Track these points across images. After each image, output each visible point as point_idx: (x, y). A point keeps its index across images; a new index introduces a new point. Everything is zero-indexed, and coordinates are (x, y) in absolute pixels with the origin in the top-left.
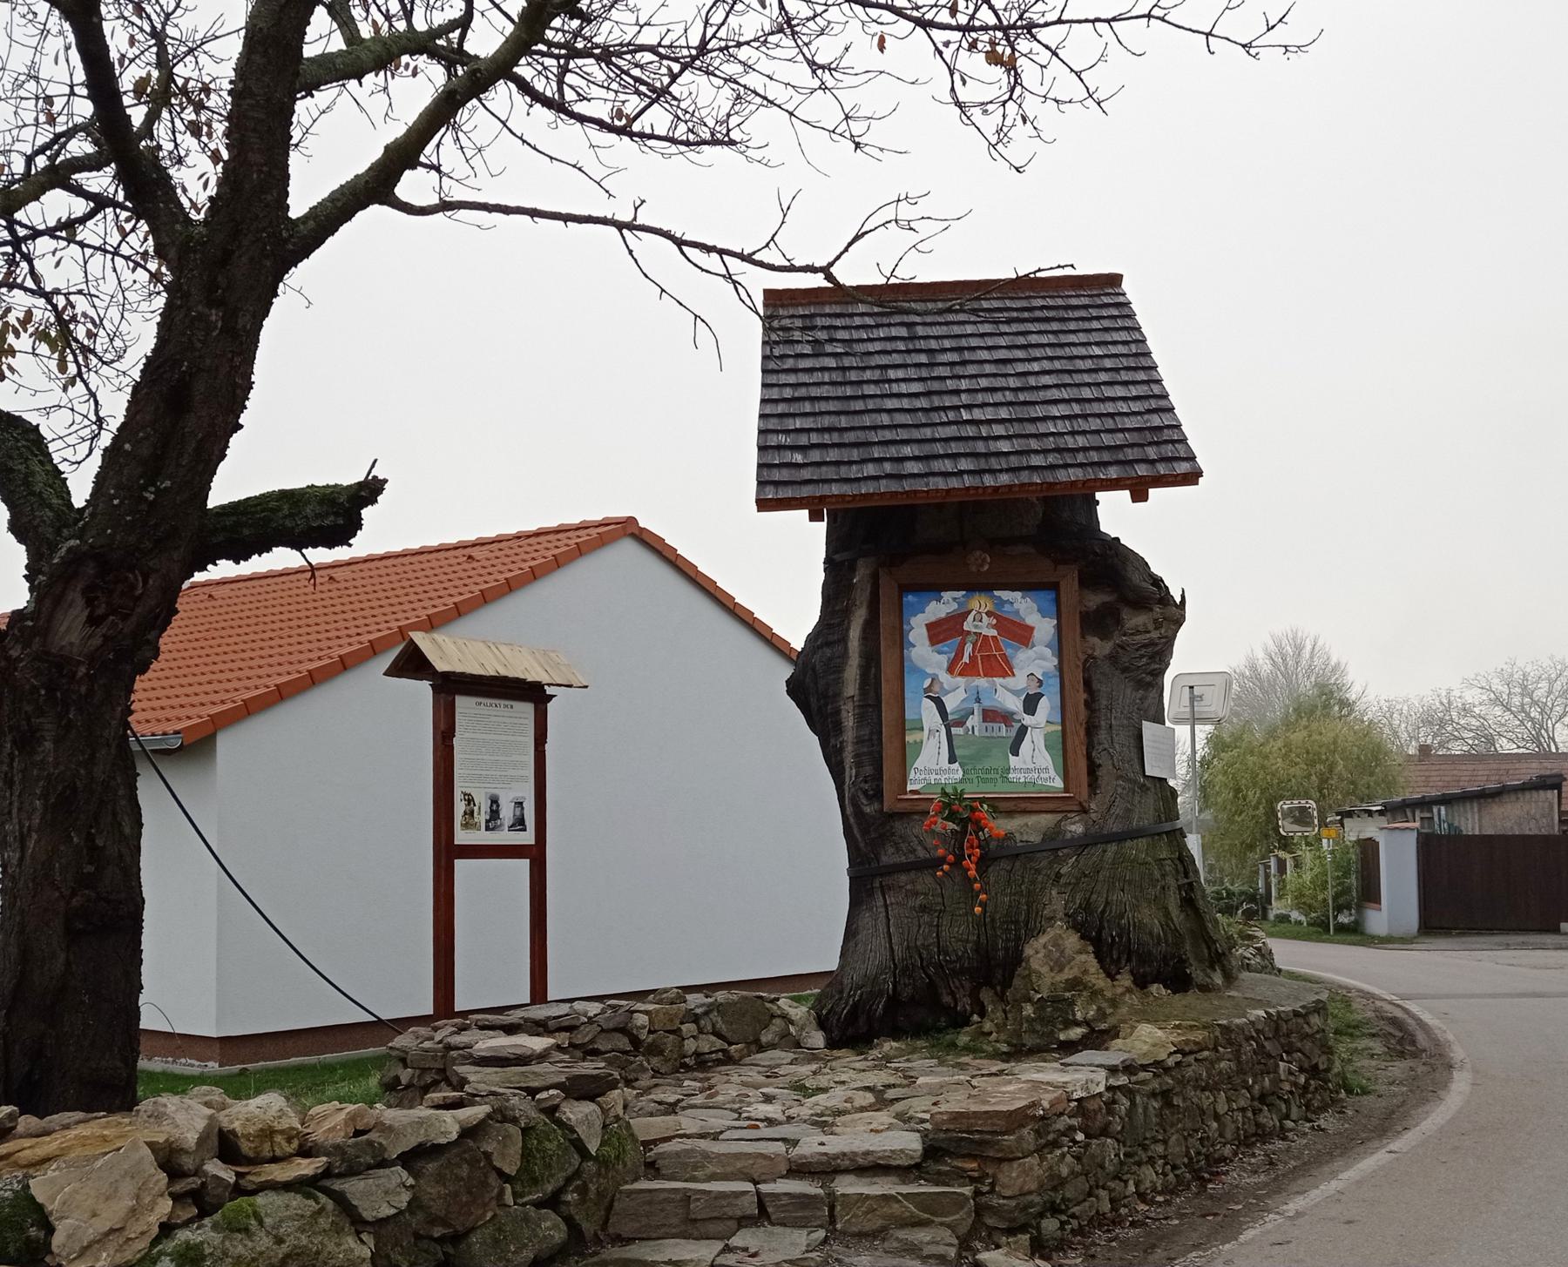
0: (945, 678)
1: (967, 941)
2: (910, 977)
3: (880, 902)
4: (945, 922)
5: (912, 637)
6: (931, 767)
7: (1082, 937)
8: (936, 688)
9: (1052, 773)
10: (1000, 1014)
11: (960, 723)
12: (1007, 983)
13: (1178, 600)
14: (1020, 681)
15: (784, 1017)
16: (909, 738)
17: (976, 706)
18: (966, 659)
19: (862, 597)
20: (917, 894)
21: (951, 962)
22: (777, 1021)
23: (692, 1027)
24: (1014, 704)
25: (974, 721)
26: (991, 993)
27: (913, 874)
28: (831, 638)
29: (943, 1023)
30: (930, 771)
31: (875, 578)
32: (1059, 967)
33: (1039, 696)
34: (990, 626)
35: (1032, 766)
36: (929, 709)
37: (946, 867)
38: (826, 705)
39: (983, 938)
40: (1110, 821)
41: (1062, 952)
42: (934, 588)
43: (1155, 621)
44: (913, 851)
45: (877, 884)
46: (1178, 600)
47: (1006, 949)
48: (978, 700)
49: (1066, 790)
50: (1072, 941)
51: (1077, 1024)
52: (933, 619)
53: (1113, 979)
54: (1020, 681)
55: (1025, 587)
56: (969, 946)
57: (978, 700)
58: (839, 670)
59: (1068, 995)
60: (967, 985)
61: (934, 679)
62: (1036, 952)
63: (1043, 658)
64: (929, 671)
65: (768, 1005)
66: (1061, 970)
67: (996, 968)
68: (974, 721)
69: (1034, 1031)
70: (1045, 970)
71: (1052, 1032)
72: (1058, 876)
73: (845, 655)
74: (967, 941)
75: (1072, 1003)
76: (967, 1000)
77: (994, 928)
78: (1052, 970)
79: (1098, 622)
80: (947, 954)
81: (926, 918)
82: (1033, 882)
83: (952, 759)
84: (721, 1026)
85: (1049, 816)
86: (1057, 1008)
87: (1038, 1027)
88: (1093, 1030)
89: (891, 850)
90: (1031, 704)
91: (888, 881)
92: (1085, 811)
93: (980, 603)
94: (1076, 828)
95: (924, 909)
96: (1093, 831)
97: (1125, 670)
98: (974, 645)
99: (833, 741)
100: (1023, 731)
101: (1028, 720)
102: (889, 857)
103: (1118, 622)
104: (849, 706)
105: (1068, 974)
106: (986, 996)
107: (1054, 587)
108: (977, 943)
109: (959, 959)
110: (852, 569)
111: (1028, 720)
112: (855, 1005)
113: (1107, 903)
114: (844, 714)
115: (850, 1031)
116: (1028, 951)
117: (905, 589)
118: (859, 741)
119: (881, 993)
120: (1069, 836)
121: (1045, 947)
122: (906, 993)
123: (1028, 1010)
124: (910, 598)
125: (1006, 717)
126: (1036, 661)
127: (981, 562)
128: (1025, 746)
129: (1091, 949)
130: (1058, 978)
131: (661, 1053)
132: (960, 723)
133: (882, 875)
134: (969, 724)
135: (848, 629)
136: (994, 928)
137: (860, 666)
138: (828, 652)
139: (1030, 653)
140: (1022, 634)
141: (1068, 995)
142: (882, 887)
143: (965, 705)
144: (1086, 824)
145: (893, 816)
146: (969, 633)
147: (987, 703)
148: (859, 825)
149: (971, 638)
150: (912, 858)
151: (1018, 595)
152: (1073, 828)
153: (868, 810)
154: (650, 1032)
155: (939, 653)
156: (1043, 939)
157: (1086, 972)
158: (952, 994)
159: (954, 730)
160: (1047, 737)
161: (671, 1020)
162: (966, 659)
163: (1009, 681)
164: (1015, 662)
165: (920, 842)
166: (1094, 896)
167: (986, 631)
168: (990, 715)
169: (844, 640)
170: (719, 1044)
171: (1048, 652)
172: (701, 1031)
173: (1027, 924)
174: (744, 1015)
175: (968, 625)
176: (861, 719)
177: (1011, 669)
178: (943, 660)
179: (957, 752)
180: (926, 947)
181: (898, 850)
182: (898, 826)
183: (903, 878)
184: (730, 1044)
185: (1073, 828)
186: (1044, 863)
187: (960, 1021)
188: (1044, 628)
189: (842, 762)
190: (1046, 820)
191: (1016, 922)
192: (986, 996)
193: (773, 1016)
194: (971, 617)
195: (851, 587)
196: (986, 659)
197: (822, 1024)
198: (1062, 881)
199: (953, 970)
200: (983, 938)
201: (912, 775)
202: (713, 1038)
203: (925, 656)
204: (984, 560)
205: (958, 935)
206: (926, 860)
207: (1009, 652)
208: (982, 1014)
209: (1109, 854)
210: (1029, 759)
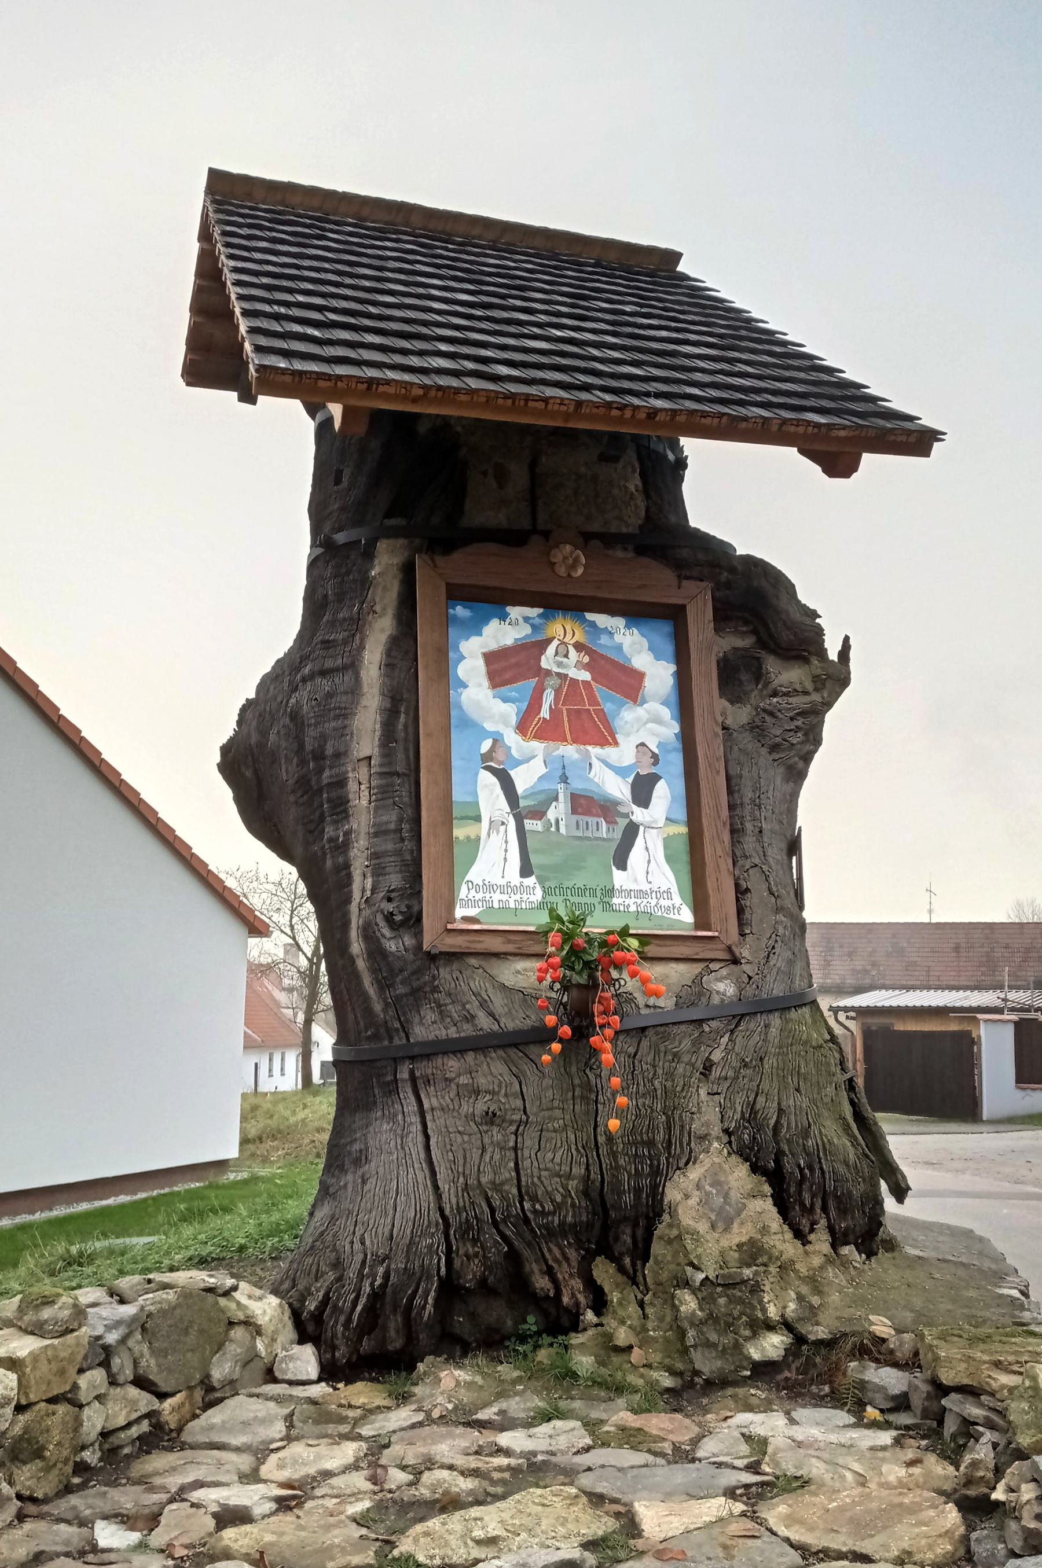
0: (512, 739)
1: (569, 1176)
2: (475, 1241)
3: (411, 1106)
4: (529, 1141)
5: (462, 671)
6: (491, 881)
7: (755, 1169)
8: (500, 755)
9: (677, 900)
10: (633, 1309)
11: (539, 814)
12: (642, 1252)
13: (833, 655)
14: (625, 753)
15: (248, 1323)
16: (459, 832)
17: (561, 788)
18: (545, 713)
19: (385, 597)
20: (477, 1092)
21: (543, 1213)
22: (238, 1333)
23: (98, 1375)
24: (619, 789)
25: (557, 811)
26: (612, 1268)
27: (470, 1057)
28: (329, 664)
29: (532, 1322)
30: (491, 887)
31: (408, 571)
32: (724, 1221)
33: (654, 778)
34: (579, 665)
35: (645, 887)
36: (488, 785)
37: (556, 1047)
38: (320, 771)
39: (594, 1169)
40: (770, 979)
41: (726, 1196)
42: (493, 599)
43: (816, 679)
44: (470, 1018)
45: (404, 1074)
46: (833, 655)
47: (638, 1191)
48: (564, 779)
49: (699, 925)
50: (739, 1176)
51: (770, 1327)
52: (493, 646)
53: (805, 1242)
54: (625, 753)
55: (636, 612)
56: (572, 1184)
57: (564, 779)
58: (345, 714)
59: (747, 1272)
60: (572, 1254)
61: (497, 740)
62: (687, 1193)
63: (658, 720)
64: (489, 726)
65: (223, 1302)
66: (727, 1229)
67: (621, 1224)
68: (557, 811)
69: (709, 1345)
70: (703, 1227)
71: (737, 1347)
72: (708, 1066)
73: (355, 691)
74: (569, 1176)
75: (756, 1289)
76: (577, 1284)
77: (614, 1155)
78: (713, 1227)
79: (734, 676)
80: (534, 1199)
81: (496, 1134)
82: (670, 1075)
83: (526, 870)
84: (150, 1364)
85: (682, 967)
86: (734, 1297)
87: (713, 1337)
88: (800, 1340)
89: (430, 1016)
90: (642, 790)
91: (422, 1069)
92: (735, 961)
93: (563, 629)
94: (724, 987)
95: (491, 1118)
96: (750, 991)
97: (774, 748)
98: (558, 692)
99: (329, 831)
100: (632, 831)
101: (639, 815)
102: (427, 1028)
103: (759, 676)
104: (363, 772)
105: (740, 1234)
106: (604, 1272)
107: (675, 616)
108: (586, 1179)
109: (558, 1207)
110: (369, 554)
111: (639, 815)
112: (376, 1296)
113: (781, 1111)
114: (352, 786)
115: (367, 1345)
116: (672, 1194)
117: (457, 594)
118: (379, 832)
119: (425, 1273)
120: (716, 1000)
121: (698, 1187)
122: (471, 1273)
123: (689, 1303)
124: (460, 611)
125: (607, 809)
126: (648, 724)
127: (571, 563)
128: (636, 855)
129: (767, 1189)
130: (725, 1243)
131: (38, 1453)
132: (539, 814)
133: (412, 1058)
134: (551, 814)
135: (362, 647)
136: (614, 1155)
137: (382, 710)
138: (325, 685)
139: (640, 712)
140: (629, 684)
141: (747, 1272)
142: (413, 1079)
143: (545, 786)
144: (738, 983)
145: (433, 958)
146: (548, 673)
147: (577, 785)
148: (374, 971)
149: (552, 682)
150: (467, 1030)
151: (619, 622)
152: (721, 986)
153: (391, 946)
154: (20, 1409)
155: (505, 700)
156: (695, 1173)
157: (765, 1230)
158: (550, 1272)
159: (529, 824)
160: (667, 842)
161: (62, 1372)
162: (545, 713)
163: (610, 753)
164: (617, 724)
165: (483, 1004)
166: (761, 1100)
167: (574, 673)
168: (586, 804)
169: (353, 666)
170: (145, 1401)
171: (666, 713)
172: (113, 1382)
173: (663, 1149)
174: (186, 1331)
175: (548, 661)
176: (383, 796)
177: (613, 735)
178: (511, 712)
179: (534, 859)
180: (497, 1187)
181: (443, 1014)
182: (445, 974)
183: (453, 1064)
184: (162, 1396)
185: (721, 986)
186: (686, 1044)
187: (561, 1323)
188: (659, 674)
189: (347, 866)
190: (678, 973)
191: (651, 1143)
192: (604, 1272)
193: (231, 1324)
194: (551, 650)
195: (365, 583)
196: (576, 715)
197: (307, 1328)
198: (716, 1073)
199: (547, 1227)
200: (594, 1169)
201: (463, 892)
202: (133, 1392)
203: (480, 702)
204: (576, 560)
205: (553, 1165)
206: (492, 1035)
207: (608, 707)
208: (600, 1304)
209: (774, 1031)
210: (641, 877)
